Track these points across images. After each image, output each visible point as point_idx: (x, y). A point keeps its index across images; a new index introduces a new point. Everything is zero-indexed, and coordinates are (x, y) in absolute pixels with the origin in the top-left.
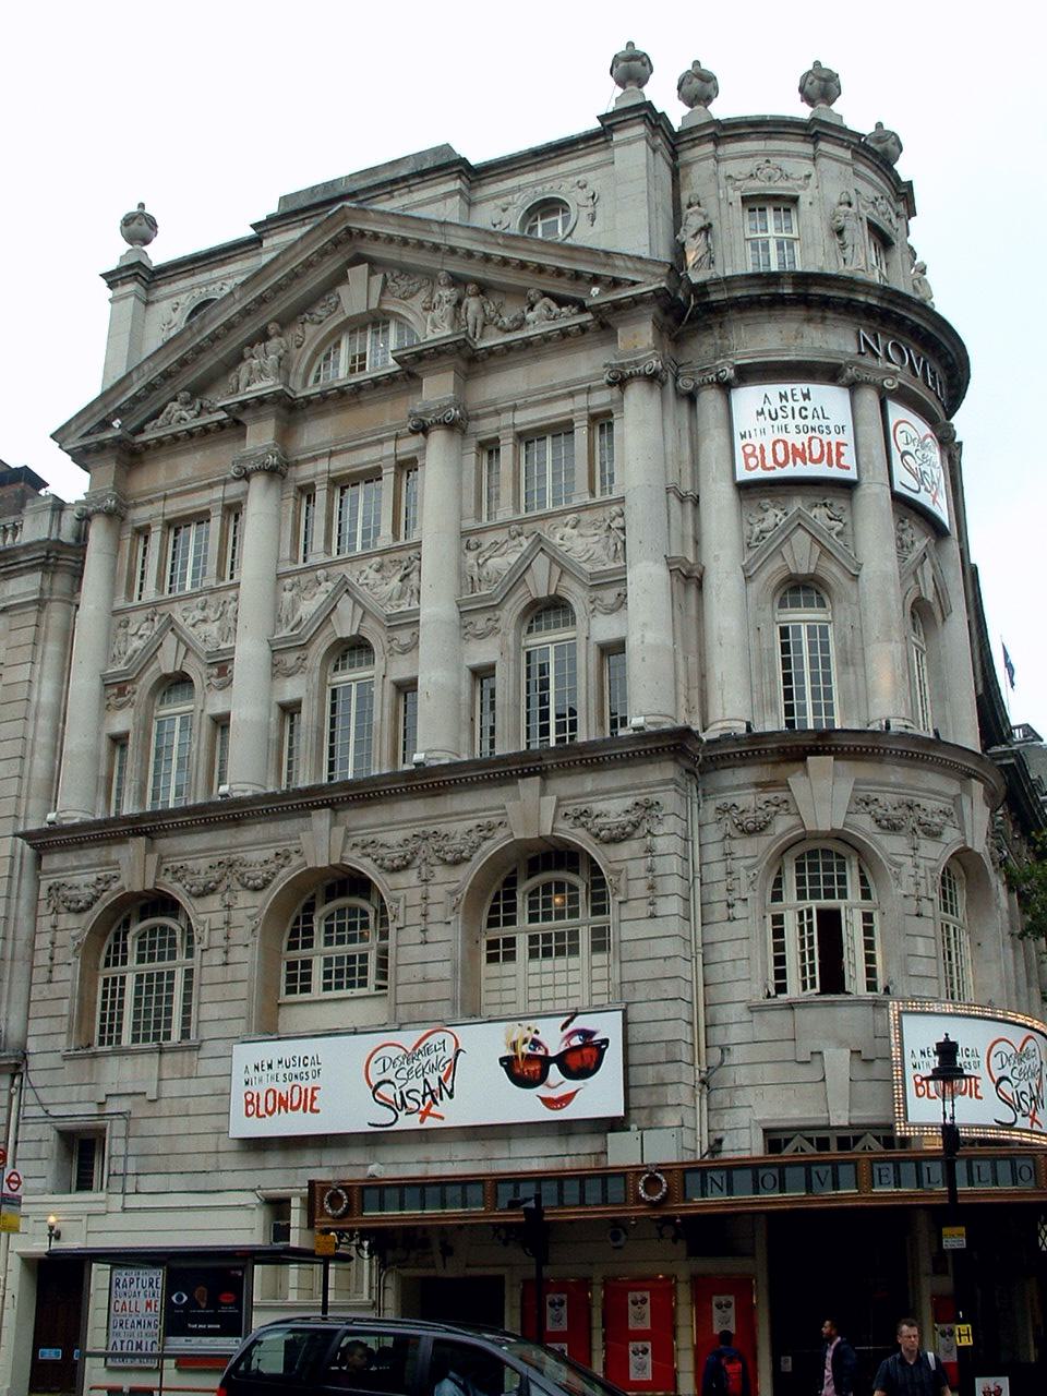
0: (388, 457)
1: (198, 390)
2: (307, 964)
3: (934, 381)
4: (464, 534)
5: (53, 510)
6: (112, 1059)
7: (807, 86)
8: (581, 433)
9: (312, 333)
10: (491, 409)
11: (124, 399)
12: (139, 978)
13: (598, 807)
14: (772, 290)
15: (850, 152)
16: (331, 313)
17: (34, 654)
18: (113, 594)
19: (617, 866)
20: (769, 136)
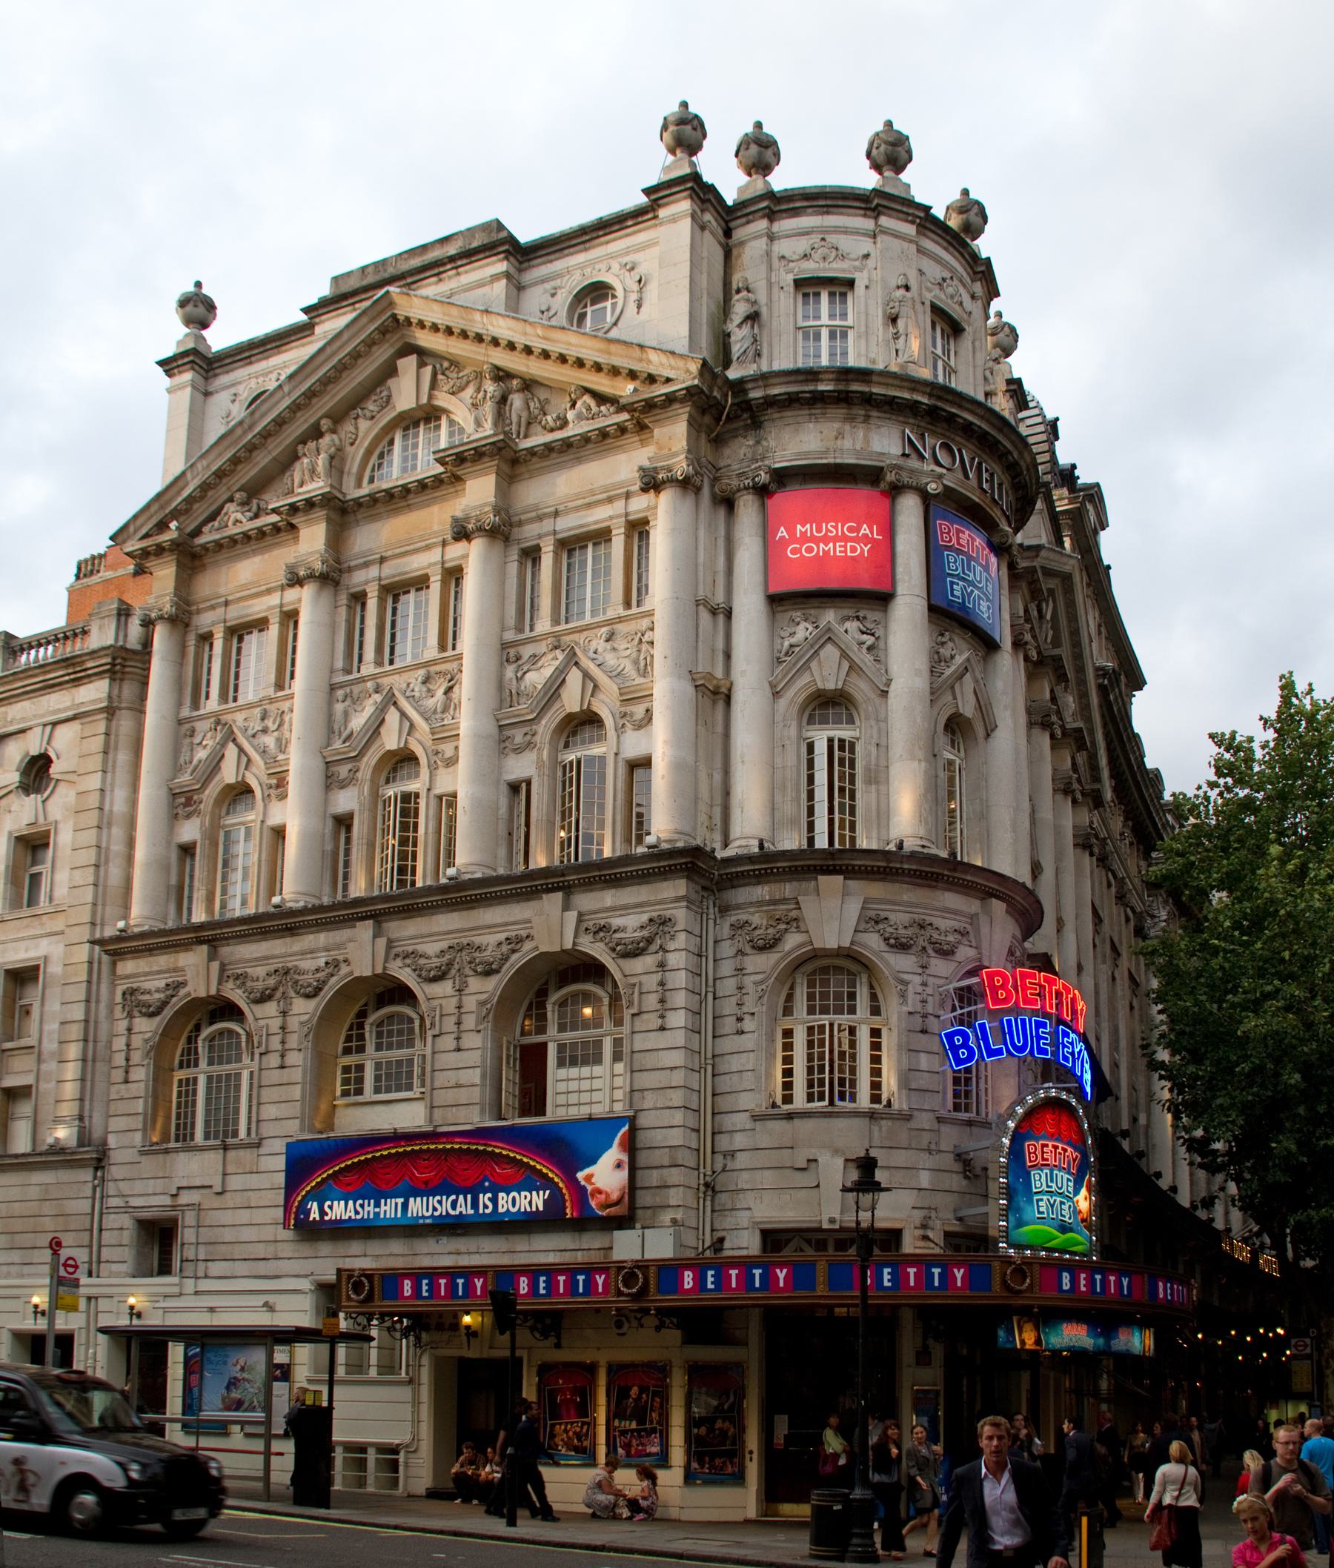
0: (435, 564)
1: (254, 491)
2: (360, 1068)
3: (991, 481)
4: (505, 646)
5: (119, 615)
6: (182, 1154)
7: (874, 152)
8: (618, 542)
9: (366, 429)
10: (534, 514)
11: (180, 499)
12: (210, 1079)
13: (617, 922)
14: (811, 388)
15: (914, 227)
16: (383, 408)
17: (105, 762)
18: (179, 704)
19: (633, 980)
20: (827, 210)
